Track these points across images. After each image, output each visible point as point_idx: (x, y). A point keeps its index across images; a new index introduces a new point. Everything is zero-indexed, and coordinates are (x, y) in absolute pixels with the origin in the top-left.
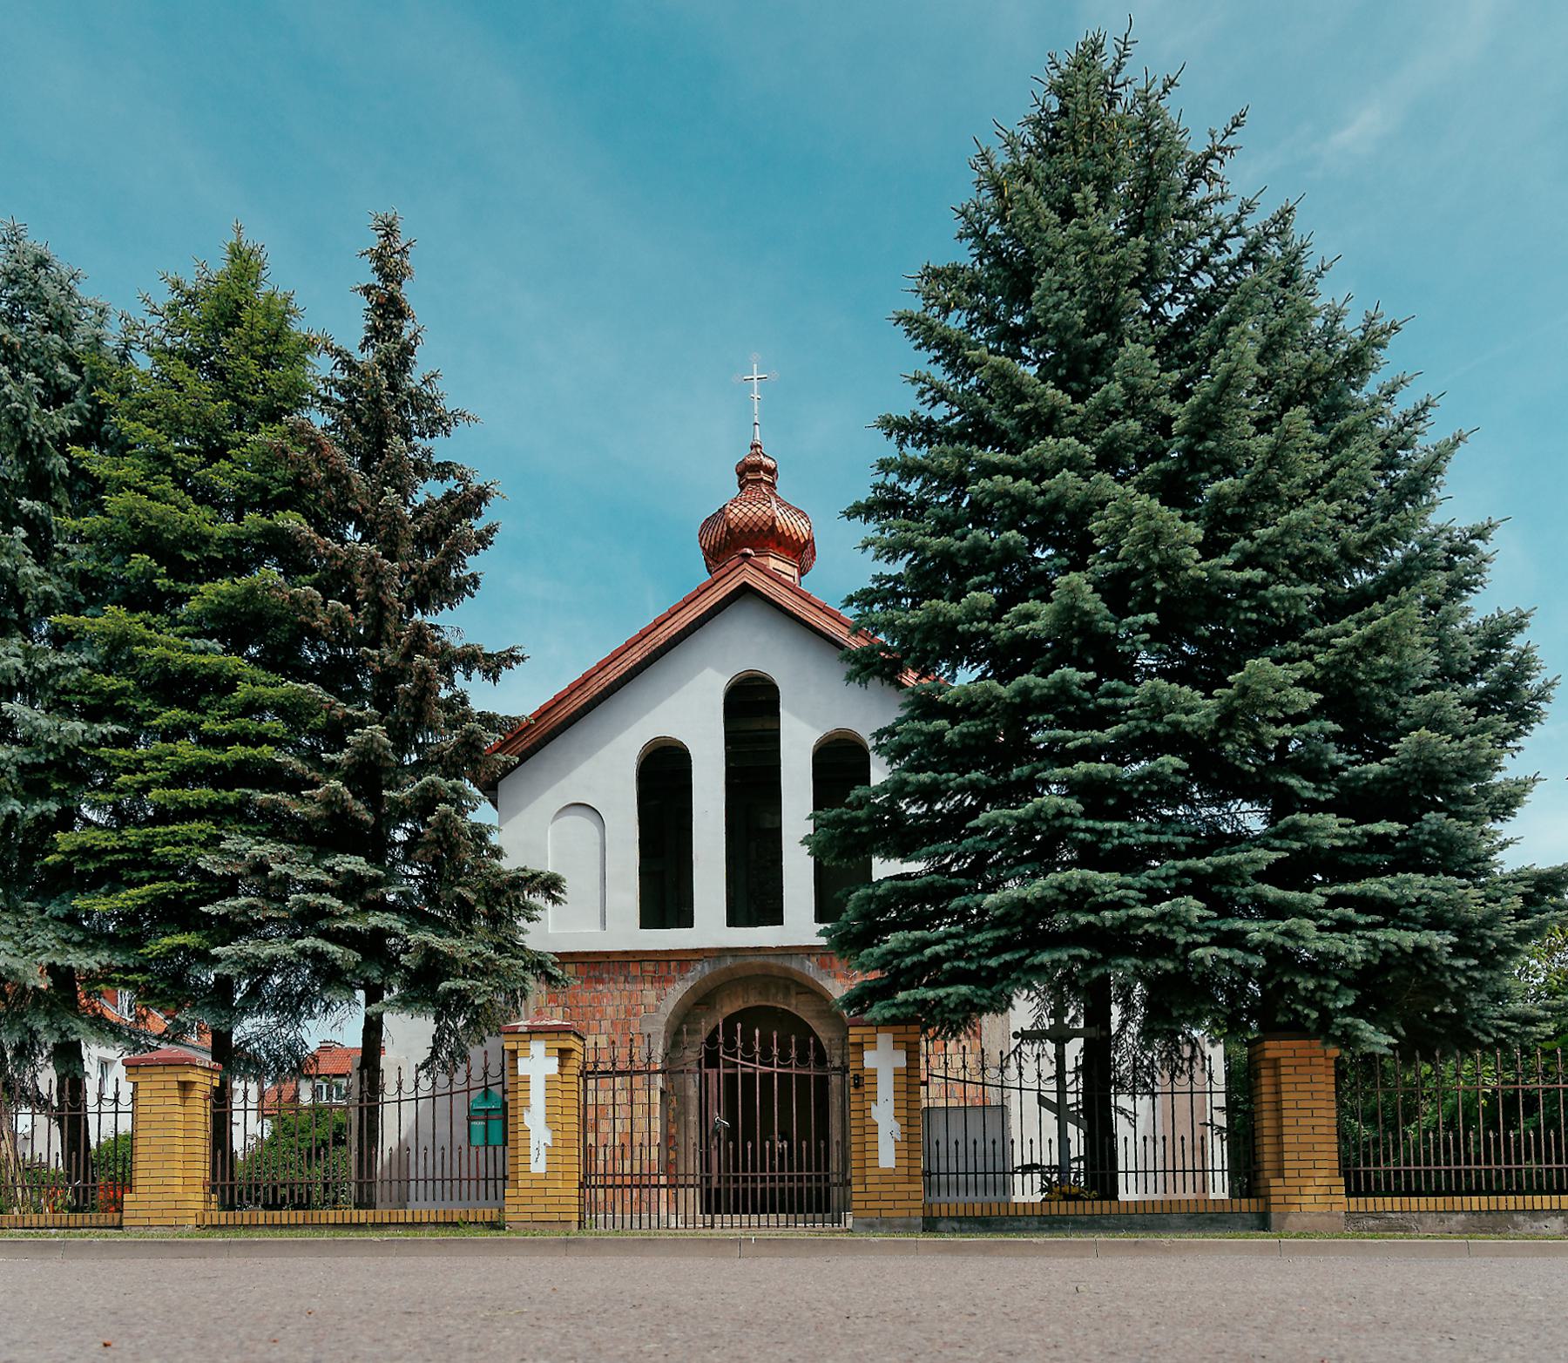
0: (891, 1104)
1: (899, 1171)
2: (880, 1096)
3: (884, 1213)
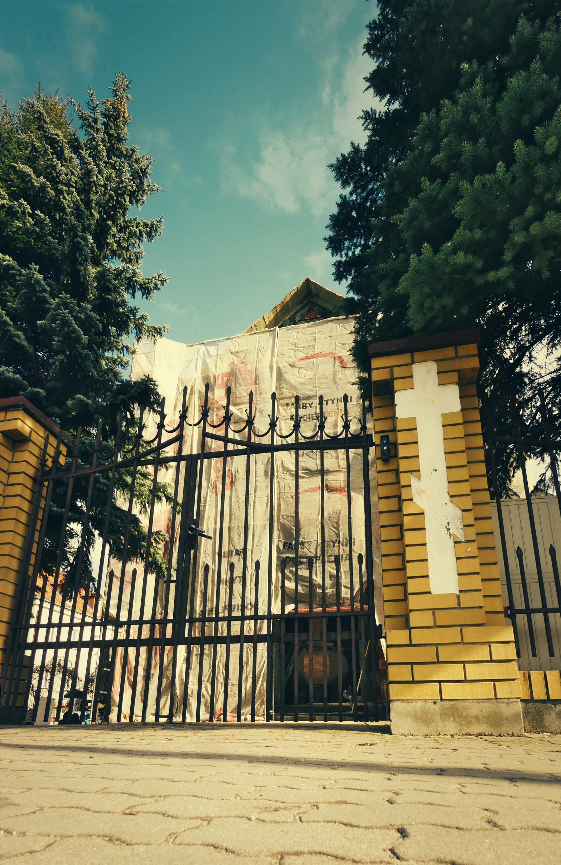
0: (442, 475)
1: (467, 600)
2: (424, 463)
3: (449, 691)
